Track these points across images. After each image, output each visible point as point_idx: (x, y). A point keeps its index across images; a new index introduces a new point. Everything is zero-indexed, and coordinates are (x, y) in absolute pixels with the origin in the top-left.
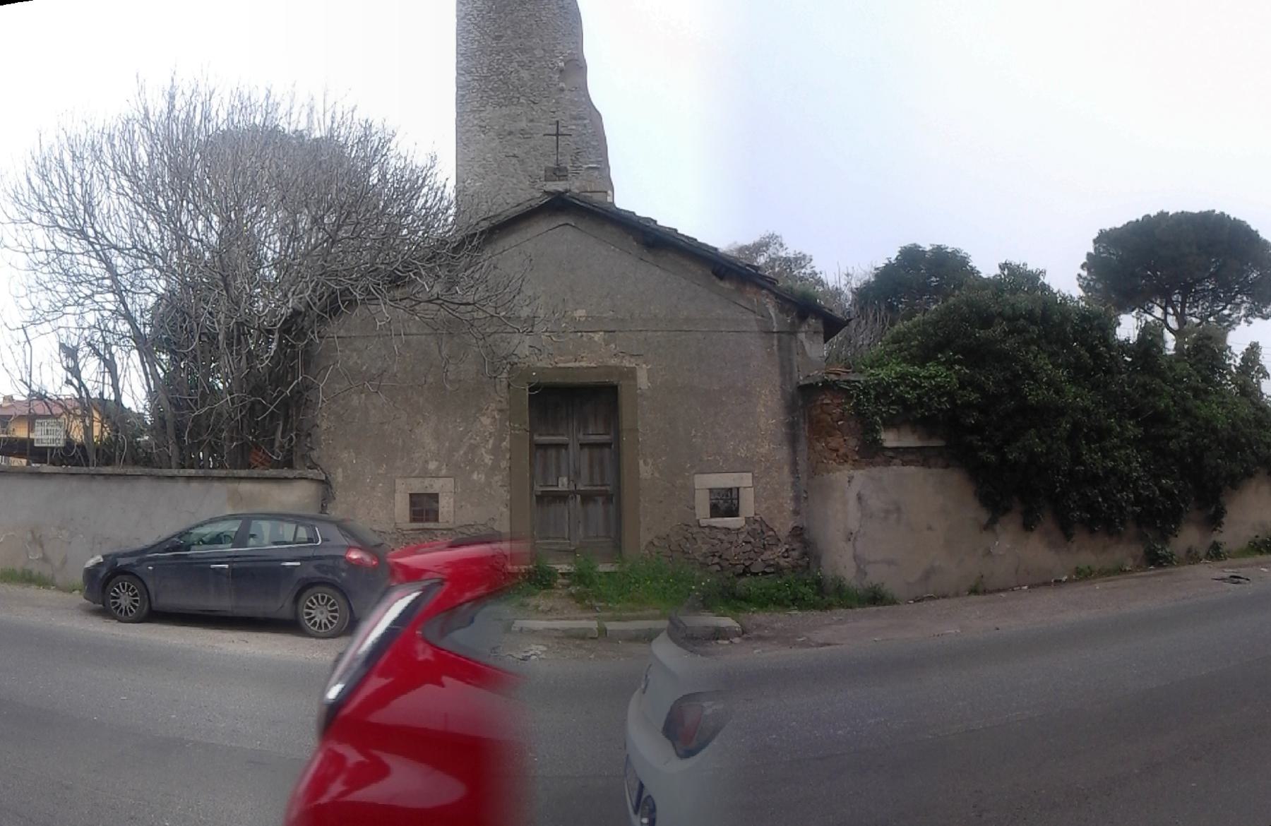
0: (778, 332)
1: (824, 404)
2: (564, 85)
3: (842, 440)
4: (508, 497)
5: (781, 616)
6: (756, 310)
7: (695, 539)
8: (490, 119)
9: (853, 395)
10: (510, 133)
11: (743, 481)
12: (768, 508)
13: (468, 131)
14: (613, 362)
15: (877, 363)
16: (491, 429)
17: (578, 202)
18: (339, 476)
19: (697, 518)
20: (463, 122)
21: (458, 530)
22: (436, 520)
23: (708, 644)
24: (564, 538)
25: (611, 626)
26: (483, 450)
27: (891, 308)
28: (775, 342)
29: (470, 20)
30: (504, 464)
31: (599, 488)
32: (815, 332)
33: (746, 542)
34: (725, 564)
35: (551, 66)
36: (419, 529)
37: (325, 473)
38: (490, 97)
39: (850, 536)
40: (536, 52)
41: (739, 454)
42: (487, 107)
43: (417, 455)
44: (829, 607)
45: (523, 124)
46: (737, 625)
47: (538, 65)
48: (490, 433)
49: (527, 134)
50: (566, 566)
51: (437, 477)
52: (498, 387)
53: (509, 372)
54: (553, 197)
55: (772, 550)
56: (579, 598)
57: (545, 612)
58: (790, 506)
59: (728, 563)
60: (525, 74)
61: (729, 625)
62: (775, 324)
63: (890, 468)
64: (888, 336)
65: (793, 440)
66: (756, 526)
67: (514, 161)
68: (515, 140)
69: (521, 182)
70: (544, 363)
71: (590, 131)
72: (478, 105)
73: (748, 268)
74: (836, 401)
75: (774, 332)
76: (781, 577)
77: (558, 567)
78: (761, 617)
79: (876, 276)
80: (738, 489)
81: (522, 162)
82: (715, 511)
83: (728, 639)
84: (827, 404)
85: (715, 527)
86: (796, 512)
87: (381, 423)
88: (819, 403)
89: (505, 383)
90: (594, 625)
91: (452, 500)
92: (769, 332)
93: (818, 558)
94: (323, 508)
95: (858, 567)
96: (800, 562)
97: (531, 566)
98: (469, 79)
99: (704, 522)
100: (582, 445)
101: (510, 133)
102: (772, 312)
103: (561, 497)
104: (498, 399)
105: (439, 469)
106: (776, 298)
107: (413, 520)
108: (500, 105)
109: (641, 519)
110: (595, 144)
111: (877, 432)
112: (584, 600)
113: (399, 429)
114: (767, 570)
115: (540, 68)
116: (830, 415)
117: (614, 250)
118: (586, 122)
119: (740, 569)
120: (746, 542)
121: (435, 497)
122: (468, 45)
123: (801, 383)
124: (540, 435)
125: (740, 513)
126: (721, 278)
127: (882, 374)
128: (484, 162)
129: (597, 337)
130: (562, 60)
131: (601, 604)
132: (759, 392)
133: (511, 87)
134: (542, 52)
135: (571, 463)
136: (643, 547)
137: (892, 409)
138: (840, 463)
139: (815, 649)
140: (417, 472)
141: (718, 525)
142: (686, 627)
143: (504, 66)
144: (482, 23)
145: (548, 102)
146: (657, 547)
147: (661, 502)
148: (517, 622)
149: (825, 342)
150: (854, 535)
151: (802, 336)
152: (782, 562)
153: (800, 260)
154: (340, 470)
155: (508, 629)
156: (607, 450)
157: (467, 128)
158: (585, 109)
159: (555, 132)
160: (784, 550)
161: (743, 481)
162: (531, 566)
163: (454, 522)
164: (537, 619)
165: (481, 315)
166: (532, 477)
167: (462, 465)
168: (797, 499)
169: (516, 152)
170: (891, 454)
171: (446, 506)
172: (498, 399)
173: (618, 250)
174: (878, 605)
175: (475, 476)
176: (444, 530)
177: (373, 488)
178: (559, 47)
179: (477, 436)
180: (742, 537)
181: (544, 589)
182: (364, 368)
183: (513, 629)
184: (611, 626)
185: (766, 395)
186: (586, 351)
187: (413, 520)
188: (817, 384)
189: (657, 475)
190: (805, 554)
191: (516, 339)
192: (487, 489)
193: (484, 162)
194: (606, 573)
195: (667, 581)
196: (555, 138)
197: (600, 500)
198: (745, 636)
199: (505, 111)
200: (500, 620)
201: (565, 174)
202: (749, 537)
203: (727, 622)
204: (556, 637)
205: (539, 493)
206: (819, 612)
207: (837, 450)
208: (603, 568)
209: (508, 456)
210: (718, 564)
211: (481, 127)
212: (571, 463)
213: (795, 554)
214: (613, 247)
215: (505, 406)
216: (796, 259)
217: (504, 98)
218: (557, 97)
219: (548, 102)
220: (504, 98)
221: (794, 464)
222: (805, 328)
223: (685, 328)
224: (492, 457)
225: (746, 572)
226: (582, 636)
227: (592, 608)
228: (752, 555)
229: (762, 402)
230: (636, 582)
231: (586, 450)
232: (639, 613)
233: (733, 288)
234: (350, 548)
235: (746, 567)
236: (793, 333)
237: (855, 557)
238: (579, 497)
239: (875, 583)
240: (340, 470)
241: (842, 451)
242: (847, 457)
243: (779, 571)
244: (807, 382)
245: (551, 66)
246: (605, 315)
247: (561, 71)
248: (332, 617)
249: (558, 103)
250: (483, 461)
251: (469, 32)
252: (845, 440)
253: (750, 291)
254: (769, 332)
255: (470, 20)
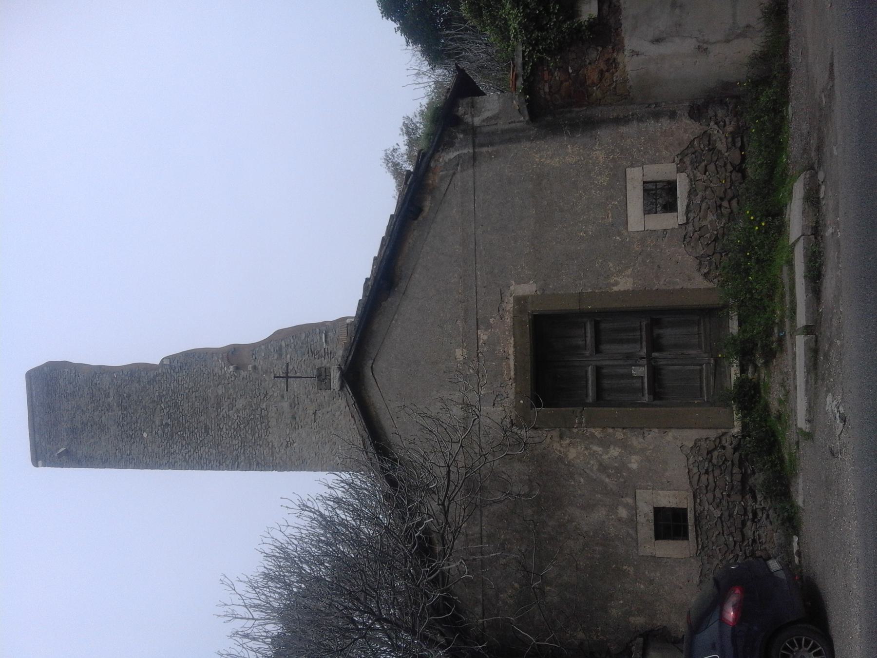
0: (474, 147)
1: (550, 91)
2: (250, 366)
3: (590, 67)
4: (656, 430)
5: (793, 125)
6: (451, 172)
7: (700, 229)
8: (280, 437)
9: (538, 58)
10: (294, 418)
11: (635, 177)
12: (666, 148)
13: (290, 459)
14: (508, 320)
15: (503, 32)
16: (581, 448)
17: (350, 358)
18: (638, 621)
19: (677, 226)
20: (281, 464)
21: (696, 487)
22: (684, 511)
23: (824, 208)
24: (701, 371)
25: (801, 320)
26: (605, 457)
27: (448, 22)
28: (484, 150)
29: (190, 456)
30: (619, 434)
31: (644, 333)
32: (473, 107)
33: (706, 171)
34: (730, 193)
35: (233, 379)
36: (696, 531)
37: (635, 638)
38: (260, 437)
39: (702, 49)
40: (220, 392)
41: (605, 184)
42: (269, 440)
43: (612, 530)
44: (786, 71)
45: (285, 405)
46: (802, 176)
47: (231, 391)
48: (586, 448)
49: (294, 401)
50: (733, 370)
51: (636, 508)
52: (537, 440)
53: (521, 428)
54: (345, 381)
55: (715, 141)
56: (770, 355)
57: (787, 393)
58: (665, 123)
59: (729, 191)
60: (240, 403)
61: (802, 186)
62: (465, 151)
63: (623, 6)
64: (474, 22)
65: (590, 124)
66: (687, 160)
67: (319, 414)
68: (300, 413)
69: (339, 408)
70: (511, 391)
71: (292, 341)
72: (267, 449)
73: (408, 183)
74: (546, 77)
75: (474, 152)
76: (748, 128)
77: (733, 378)
78: (794, 148)
79: (415, 42)
80: (644, 183)
81: (321, 406)
82: (670, 207)
83: (819, 185)
84: (550, 87)
85: (688, 206)
86: (673, 115)
87: (577, 569)
88: (548, 97)
89: (532, 433)
90: (800, 340)
91: (660, 492)
92: (474, 157)
93: (726, 86)
94: (676, 642)
95: (738, 36)
96: (731, 107)
97: (734, 406)
98: (243, 458)
99: (682, 219)
100: (598, 351)
101: (294, 418)
102: (452, 155)
103: (655, 373)
104: (548, 440)
105: (626, 506)
106: (439, 151)
107: (685, 536)
108: (268, 427)
109: (678, 287)
110: (303, 336)
111: (580, 25)
112: (771, 349)
113: (584, 549)
114: (739, 144)
115: (234, 389)
116: (562, 82)
117: (396, 321)
118: (283, 344)
119: (737, 176)
120: (706, 171)
121: (658, 511)
122: (212, 459)
123: (527, 118)
124: (587, 395)
125: (673, 178)
126: (420, 210)
127: (514, 25)
128: (319, 444)
129: (483, 336)
130: (228, 368)
131: (776, 331)
132: (538, 165)
133: (252, 417)
134: (220, 386)
135: (616, 363)
136: (711, 285)
137: (554, 8)
138: (616, 68)
139: (836, 81)
140: (631, 531)
141: (685, 203)
142: (803, 235)
143: (233, 424)
144: (194, 445)
145: (266, 381)
146: (710, 270)
147: (659, 267)
148: (799, 425)
149: (485, 94)
150: (701, 44)
151: (477, 121)
152: (730, 129)
153: (409, 130)
154: (632, 619)
155: (809, 436)
156: (603, 326)
157: (288, 459)
158: (272, 345)
159: (284, 380)
160: (716, 127)
161: (635, 177)
162: (734, 406)
163: (687, 490)
164: (796, 402)
165: (460, 457)
166: (633, 404)
167: (622, 480)
168: (656, 116)
169: (311, 412)
170: (605, 7)
171: (667, 500)
172: (548, 440)
173: (396, 317)
174: (787, 8)
175: (634, 466)
176: (695, 502)
177: (651, 582)
178: (216, 370)
179: (589, 463)
180: (699, 176)
181: (760, 393)
182: (516, 585)
183: (807, 430)
184: (801, 320)
185: (541, 157)
186: (498, 348)
187: (685, 536)
188: (527, 101)
189: (629, 272)
190: (722, 103)
191: (484, 420)
192: (648, 453)
193: (319, 444)
194: (740, 325)
195: (749, 258)
196: (289, 380)
197: (657, 331)
198: (816, 166)
199: (273, 423)
200: (798, 443)
201: (324, 369)
202: (699, 168)
203: (799, 189)
204: (816, 383)
205: (652, 397)
206: (792, 81)
207: (602, 73)
208: (734, 327)
209: (610, 430)
210: (729, 202)
211: (287, 446)
212: (616, 363)
213: (721, 113)
214: (393, 322)
215: (556, 433)
216: (408, 133)
217: (261, 424)
218: (261, 373)
219: (266, 381)
220: (261, 424)
221: (618, 121)
222: (468, 118)
223: (472, 246)
224: (612, 447)
225: (740, 169)
226: (814, 352)
227: (781, 341)
228: (721, 163)
229: (548, 161)
230: (750, 292)
231: (605, 347)
232: (787, 288)
233: (429, 198)
234: (722, 620)
235: (734, 169)
236: (473, 131)
237: (727, 41)
238: (655, 354)
239: (758, 13)
240: (632, 619)
241: (603, 66)
242: (609, 59)
243: (740, 133)
244: (526, 112)
245: (233, 379)
246: (461, 329)
247: (237, 368)
248: (806, 646)
249: (267, 371)
250: (616, 458)
251: (200, 458)
252: (590, 64)
253: (433, 180)
254: (474, 157)
255: (190, 456)
